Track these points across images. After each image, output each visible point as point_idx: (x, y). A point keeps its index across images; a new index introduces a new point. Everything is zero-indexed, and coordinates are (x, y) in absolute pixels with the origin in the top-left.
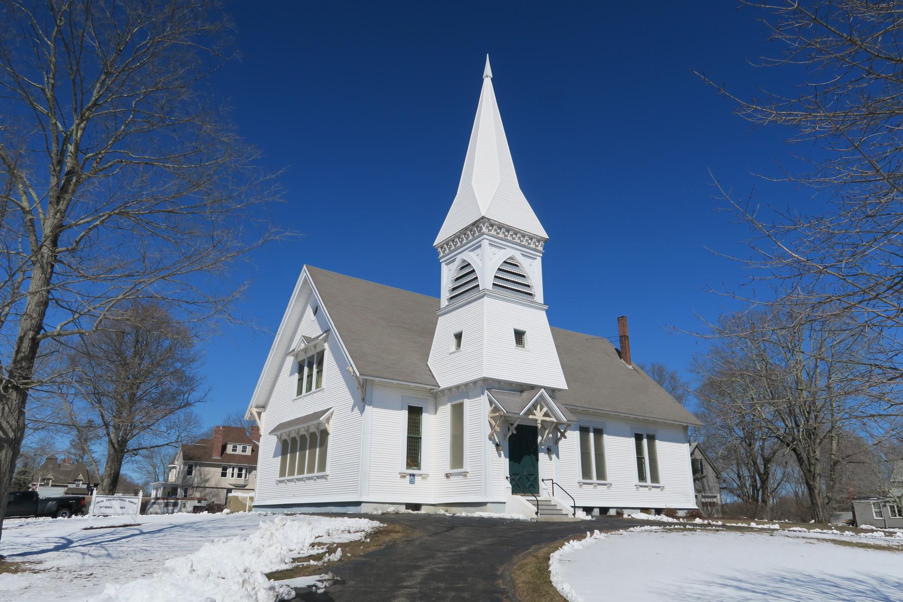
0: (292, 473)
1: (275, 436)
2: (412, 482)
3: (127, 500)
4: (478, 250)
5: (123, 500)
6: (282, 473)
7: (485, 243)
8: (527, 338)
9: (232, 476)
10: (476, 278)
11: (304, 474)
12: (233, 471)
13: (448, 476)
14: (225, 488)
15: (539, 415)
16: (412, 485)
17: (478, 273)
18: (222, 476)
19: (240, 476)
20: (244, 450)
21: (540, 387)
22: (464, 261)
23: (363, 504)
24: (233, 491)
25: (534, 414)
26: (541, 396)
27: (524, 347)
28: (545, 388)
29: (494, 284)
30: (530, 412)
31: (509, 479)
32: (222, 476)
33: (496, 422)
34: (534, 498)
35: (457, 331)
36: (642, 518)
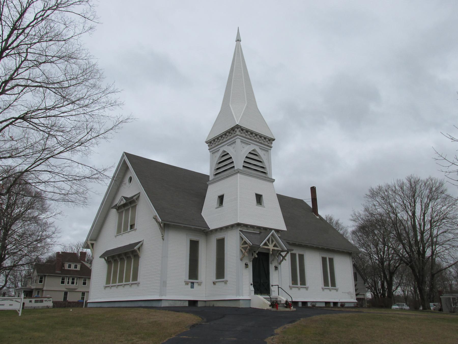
0: (114, 281)
1: (103, 259)
2: (192, 287)
3: (14, 300)
4: (233, 145)
5: (11, 300)
6: (108, 281)
7: (238, 141)
8: (264, 198)
9: (68, 283)
10: (233, 162)
11: (130, 281)
12: (69, 280)
13: (214, 283)
14: (81, 292)
15: (271, 247)
16: (192, 289)
17: (234, 159)
18: (62, 283)
19: (73, 283)
20: (76, 267)
21: (271, 229)
22: (225, 151)
23: (163, 301)
24: (301, 289)
25: (268, 246)
26: (273, 235)
27: (261, 205)
28: (274, 229)
29: (244, 166)
30: (265, 244)
31: (252, 285)
32: (62, 283)
33: (245, 251)
34: (268, 297)
35: (220, 194)
36: (287, 310)
